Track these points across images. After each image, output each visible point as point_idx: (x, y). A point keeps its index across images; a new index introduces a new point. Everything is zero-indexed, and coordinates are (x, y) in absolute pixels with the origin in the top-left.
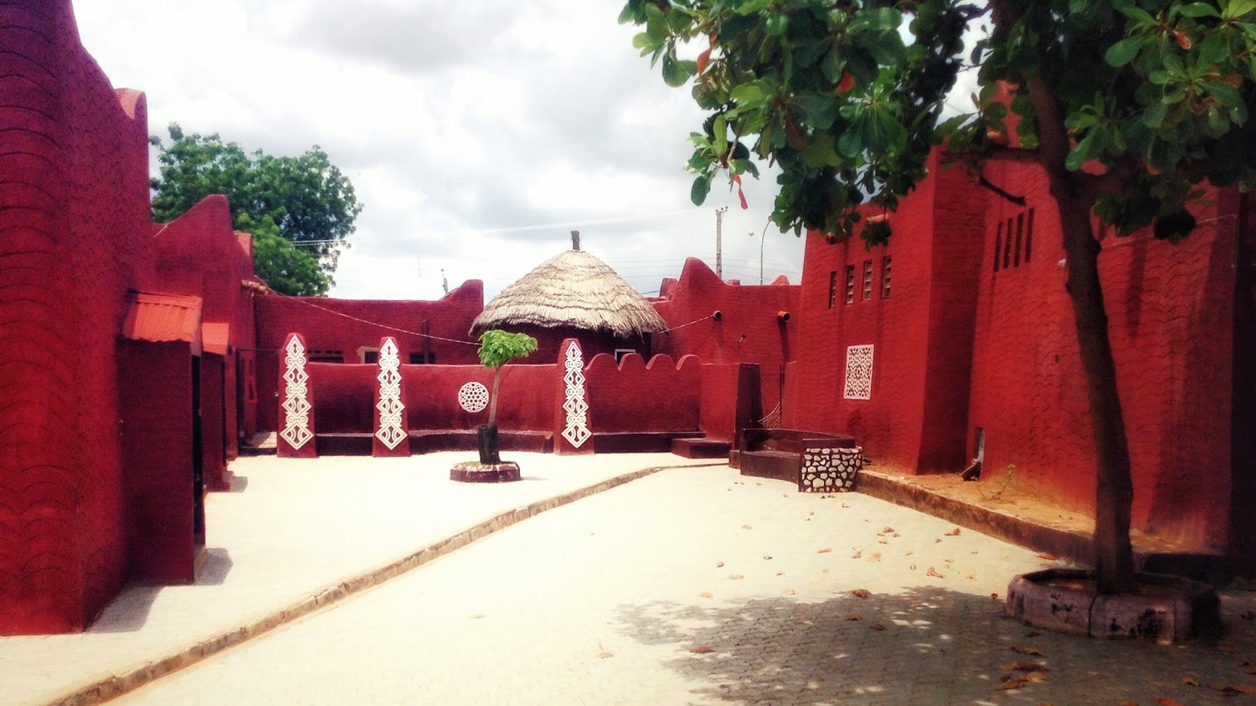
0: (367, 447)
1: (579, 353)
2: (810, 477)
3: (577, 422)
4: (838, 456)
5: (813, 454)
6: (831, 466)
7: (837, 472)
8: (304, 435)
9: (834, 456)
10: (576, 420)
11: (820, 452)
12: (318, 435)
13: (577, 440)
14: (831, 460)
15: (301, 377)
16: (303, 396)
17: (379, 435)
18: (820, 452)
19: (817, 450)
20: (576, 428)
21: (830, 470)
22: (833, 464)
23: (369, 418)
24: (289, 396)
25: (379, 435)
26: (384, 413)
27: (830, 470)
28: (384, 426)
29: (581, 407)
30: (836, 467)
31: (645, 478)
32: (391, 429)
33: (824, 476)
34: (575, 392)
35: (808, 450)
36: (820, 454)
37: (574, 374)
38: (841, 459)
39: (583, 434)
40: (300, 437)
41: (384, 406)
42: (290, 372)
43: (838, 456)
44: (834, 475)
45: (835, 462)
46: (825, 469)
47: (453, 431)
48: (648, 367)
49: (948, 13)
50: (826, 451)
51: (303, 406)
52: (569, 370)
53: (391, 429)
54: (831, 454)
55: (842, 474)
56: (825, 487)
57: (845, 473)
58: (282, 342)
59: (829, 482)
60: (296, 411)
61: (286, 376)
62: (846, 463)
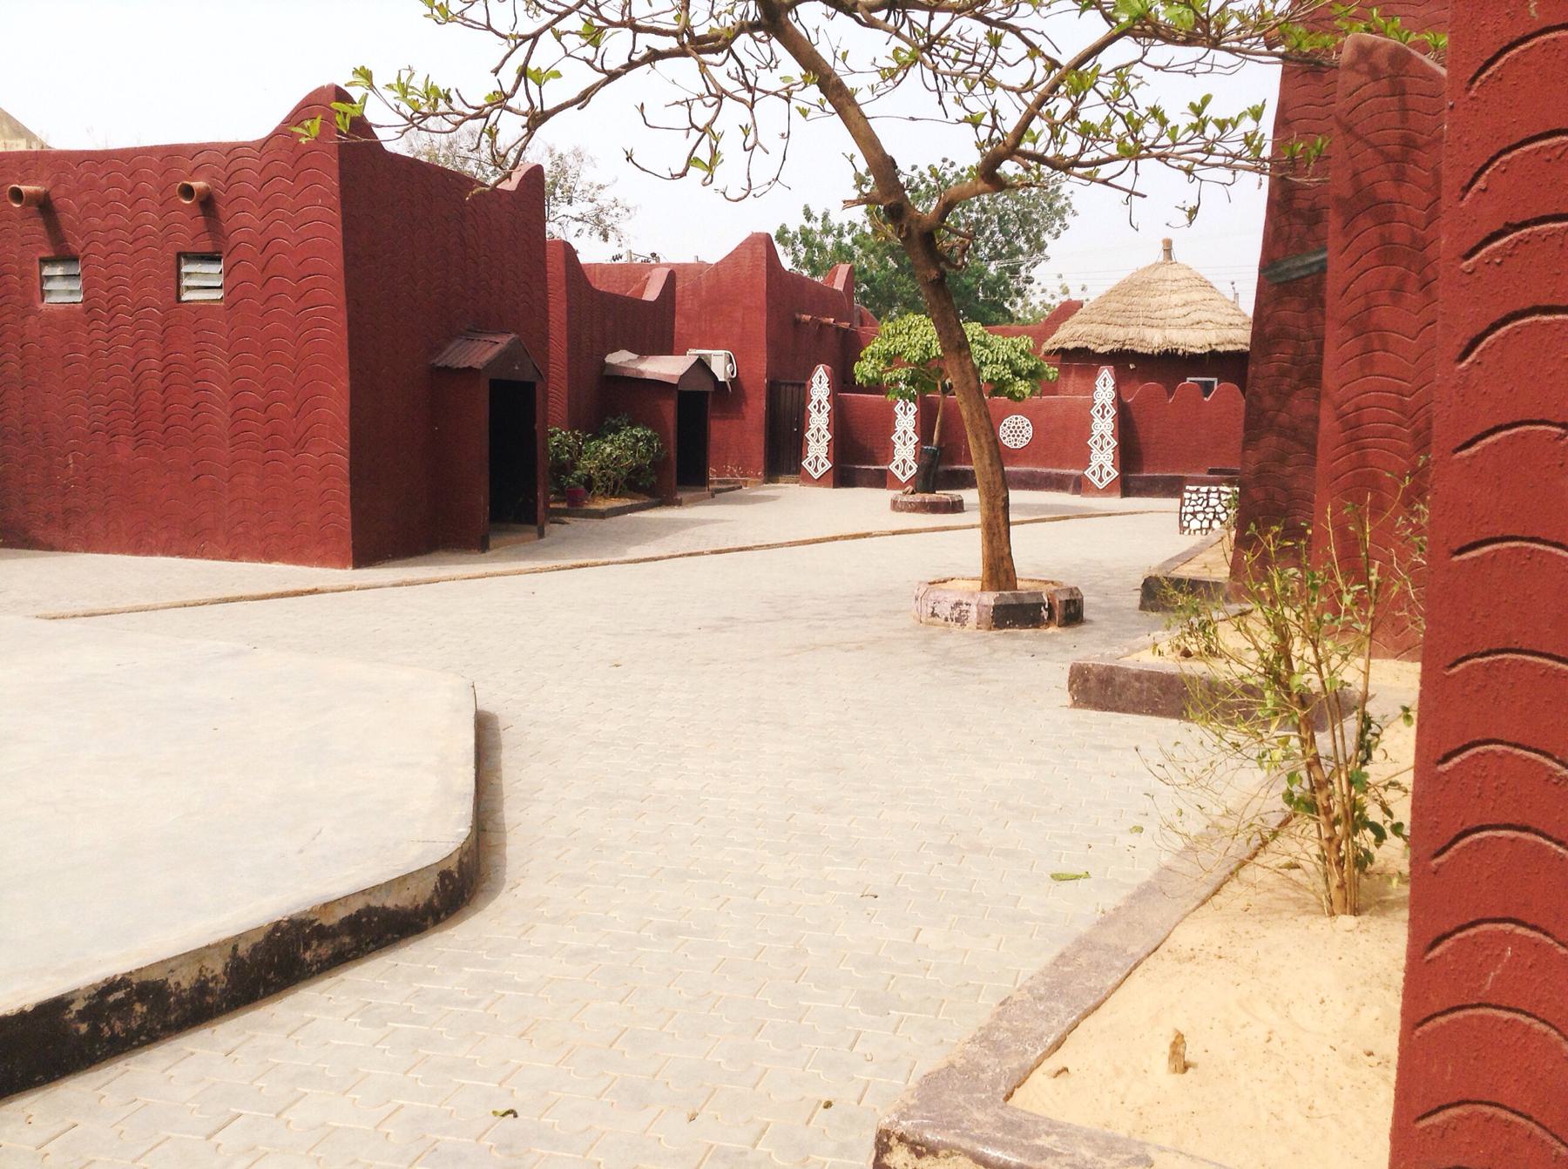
0: (1080, 485)
1: (1111, 382)
2: (1189, 517)
3: (1103, 459)
4: (1216, 495)
5: (1191, 492)
6: (1208, 505)
7: (1215, 513)
8: (823, 465)
9: (1211, 495)
10: (1102, 458)
11: (1198, 490)
12: (1078, 472)
13: (1101, 480)
14: (1208, 499)
15: (824, 408)
16: (825, 427)
17: (892, 467)
18: (1198, 490)
19: (1195, 488)
20: (1101, 467)
21: (1207, 510)
22: (1210, 504)
23: (798, 446)
24: (812, 426)
25: (892, 467)
26: (898, 445)
27: (1207, 510)
28: (898, 459)
29: (1109, 443)
30: (1214, 507)
31: (1070, 521)
32: (904, 461)
33: (1200, 516)
34: (1104, 427)
35: (1187, 487)
36: (1197, 491)
37: (1103, 407)
38: (1219, 498)
39: (1109, 474)
40: (819, 467)
41: (899, 438)
42: (815, 402)
43: (1216, 495)
44: (1210, 516)
45: (1213, 502)
46: (1201, 509)
47: (963, 467)
48: (1170, 401)
49: (89, 306)
50: (1204, 489)
51: (911, 439)
52: (1097, 401)
53: (904, 461)
54: (1208, 492)
55: (1221, 516)
56: (1201, 529)
57: (1225, 515)
58: (809, 374)
59: (1206, 524)
60: (905, 444)
61: (810, 407)
62: (1225, 503)
